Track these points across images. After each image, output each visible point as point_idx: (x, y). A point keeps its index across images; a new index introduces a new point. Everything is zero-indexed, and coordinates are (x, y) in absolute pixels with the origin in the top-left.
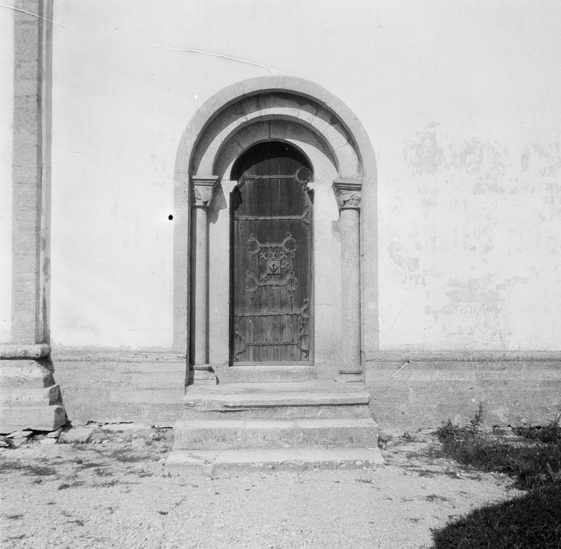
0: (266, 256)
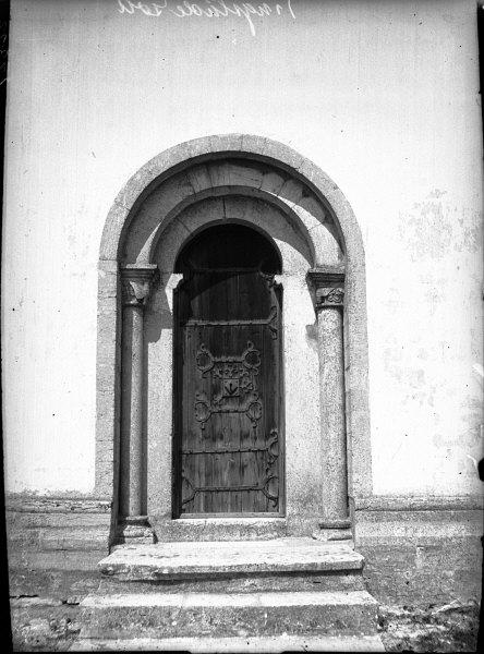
0: (221, 372)
